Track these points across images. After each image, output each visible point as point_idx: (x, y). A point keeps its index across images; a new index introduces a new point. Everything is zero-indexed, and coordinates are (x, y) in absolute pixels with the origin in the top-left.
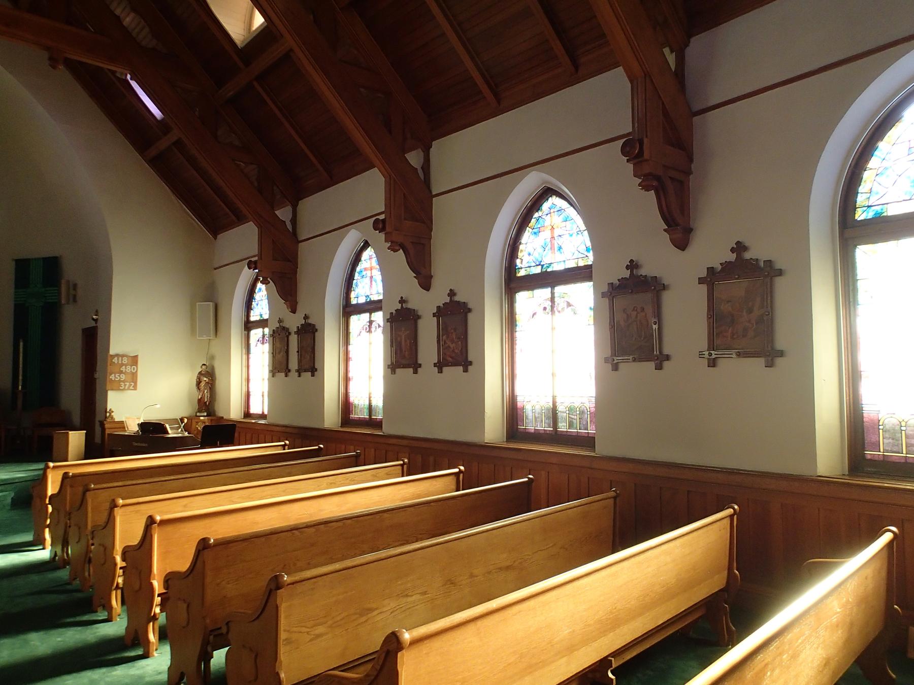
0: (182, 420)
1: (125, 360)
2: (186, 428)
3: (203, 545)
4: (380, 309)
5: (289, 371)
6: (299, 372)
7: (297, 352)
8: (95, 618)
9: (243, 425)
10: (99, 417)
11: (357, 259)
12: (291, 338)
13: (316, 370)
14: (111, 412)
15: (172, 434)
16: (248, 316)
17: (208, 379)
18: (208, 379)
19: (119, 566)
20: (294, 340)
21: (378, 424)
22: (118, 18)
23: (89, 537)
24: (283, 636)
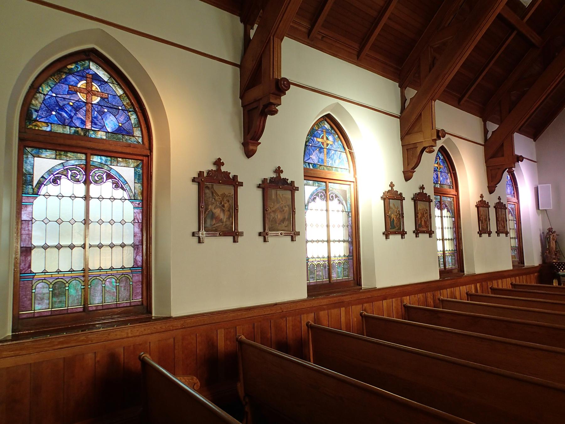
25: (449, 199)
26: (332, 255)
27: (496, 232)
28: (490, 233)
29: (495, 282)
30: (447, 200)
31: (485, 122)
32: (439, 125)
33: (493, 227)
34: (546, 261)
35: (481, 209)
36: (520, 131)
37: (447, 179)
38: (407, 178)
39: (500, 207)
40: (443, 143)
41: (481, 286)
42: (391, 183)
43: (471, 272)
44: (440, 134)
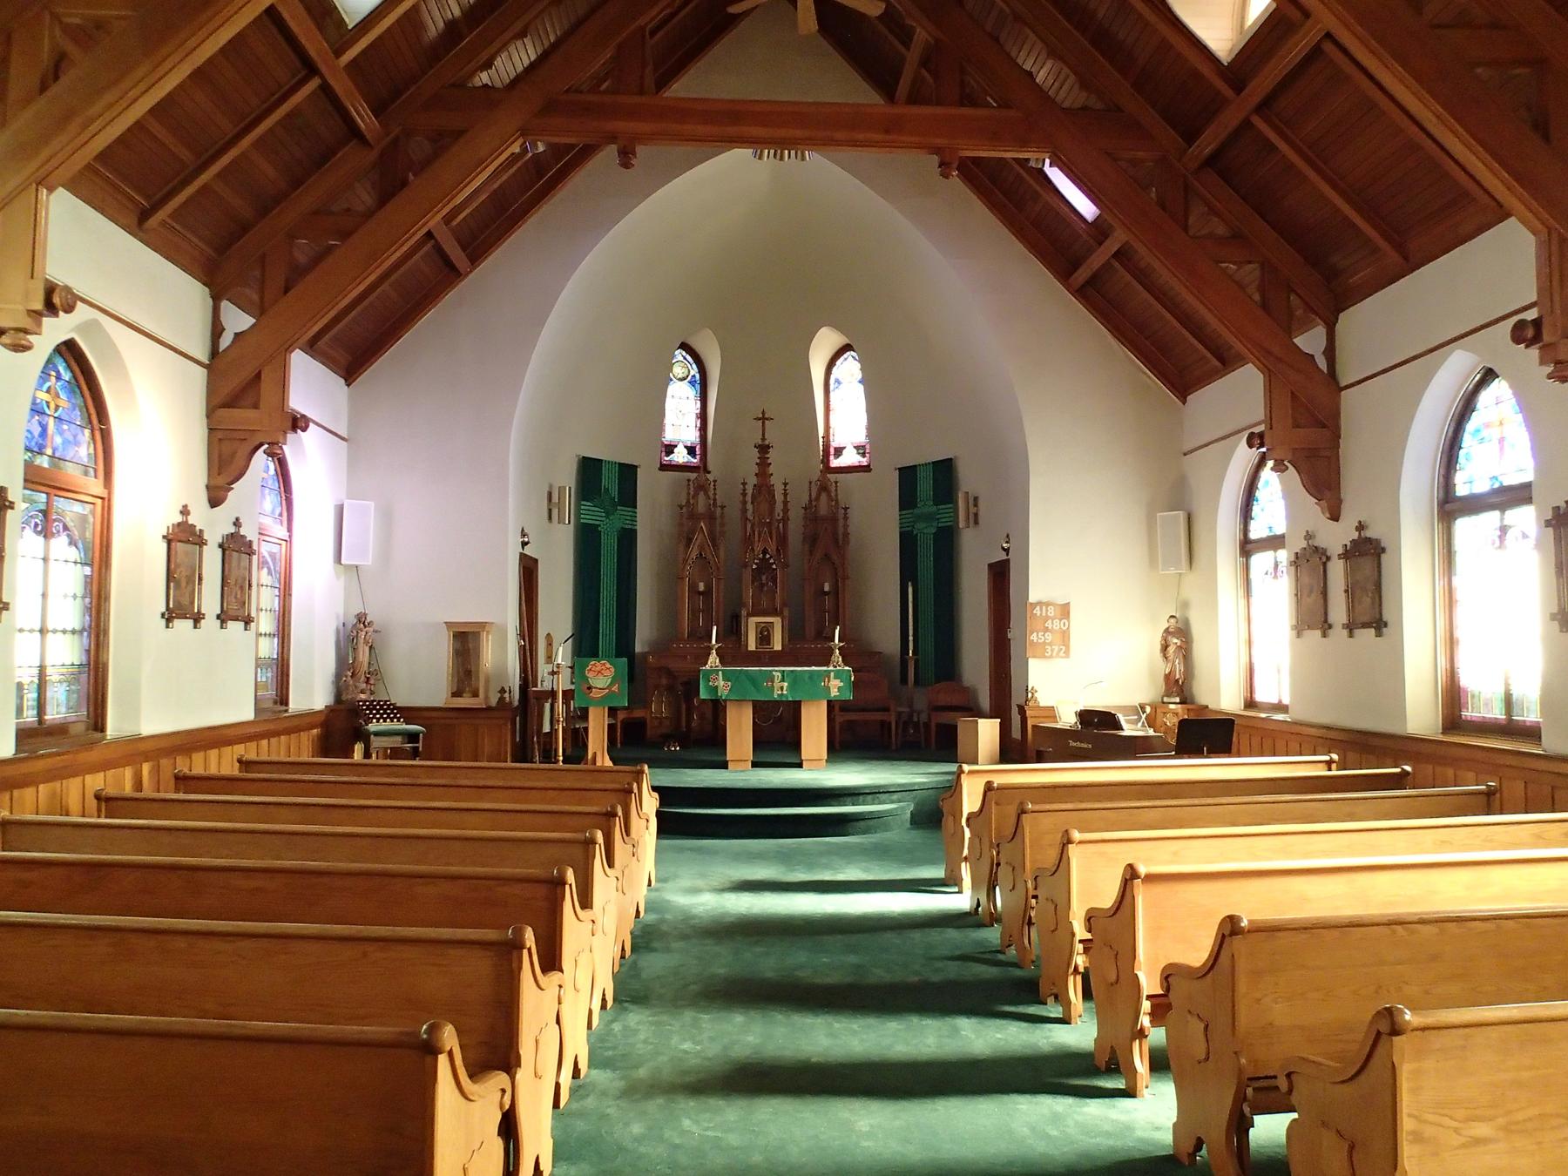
0: (1143, 707)
1: (1051, 611)
2: (1151, 722)
3: (1230, 928)
4: (1528, 500)
5: (1330, 627)
6: (1351, 628)
7: (1350, 587)
8: (1045, 1014)
9: (1243, 722)
10: (1016, 700)
11: (1467, 407)
12: (1330, 565)
13: (1386, 625)
14: (1034, 691)
15: (1128, 730)
16: (1246, 531)
17: (1179, 639)
18: (1179, 639)
19: (1078, 938)
20: (1337, 572)
21: (1531, 733)
22: (1030, 74)
23: (1030, 885)
24: (1407, 1124)
25: (78, 508)
26: (48, 662)
27: (218, 617)
28: (197, 619)
29: (198, 757)
30: (69, 509)
31: (216, 298)
32: (58, 269)
33: (210, 599)
34: (344, 698)
35: (180, 547)
36: (311, 348)
37: (77, 444)
38: (215, 502)
39: (236, 546)
40: (78, 329)
41: (156, 770)
42: (185, 507)
43: (128, 730)
44: (55, 301)
